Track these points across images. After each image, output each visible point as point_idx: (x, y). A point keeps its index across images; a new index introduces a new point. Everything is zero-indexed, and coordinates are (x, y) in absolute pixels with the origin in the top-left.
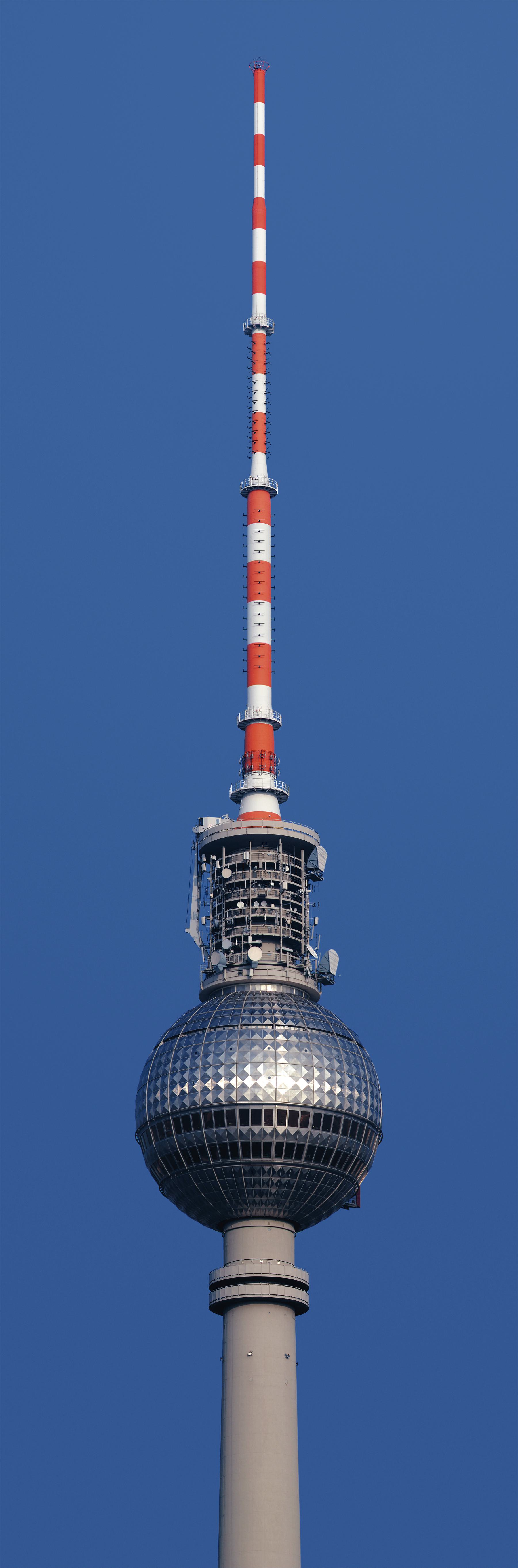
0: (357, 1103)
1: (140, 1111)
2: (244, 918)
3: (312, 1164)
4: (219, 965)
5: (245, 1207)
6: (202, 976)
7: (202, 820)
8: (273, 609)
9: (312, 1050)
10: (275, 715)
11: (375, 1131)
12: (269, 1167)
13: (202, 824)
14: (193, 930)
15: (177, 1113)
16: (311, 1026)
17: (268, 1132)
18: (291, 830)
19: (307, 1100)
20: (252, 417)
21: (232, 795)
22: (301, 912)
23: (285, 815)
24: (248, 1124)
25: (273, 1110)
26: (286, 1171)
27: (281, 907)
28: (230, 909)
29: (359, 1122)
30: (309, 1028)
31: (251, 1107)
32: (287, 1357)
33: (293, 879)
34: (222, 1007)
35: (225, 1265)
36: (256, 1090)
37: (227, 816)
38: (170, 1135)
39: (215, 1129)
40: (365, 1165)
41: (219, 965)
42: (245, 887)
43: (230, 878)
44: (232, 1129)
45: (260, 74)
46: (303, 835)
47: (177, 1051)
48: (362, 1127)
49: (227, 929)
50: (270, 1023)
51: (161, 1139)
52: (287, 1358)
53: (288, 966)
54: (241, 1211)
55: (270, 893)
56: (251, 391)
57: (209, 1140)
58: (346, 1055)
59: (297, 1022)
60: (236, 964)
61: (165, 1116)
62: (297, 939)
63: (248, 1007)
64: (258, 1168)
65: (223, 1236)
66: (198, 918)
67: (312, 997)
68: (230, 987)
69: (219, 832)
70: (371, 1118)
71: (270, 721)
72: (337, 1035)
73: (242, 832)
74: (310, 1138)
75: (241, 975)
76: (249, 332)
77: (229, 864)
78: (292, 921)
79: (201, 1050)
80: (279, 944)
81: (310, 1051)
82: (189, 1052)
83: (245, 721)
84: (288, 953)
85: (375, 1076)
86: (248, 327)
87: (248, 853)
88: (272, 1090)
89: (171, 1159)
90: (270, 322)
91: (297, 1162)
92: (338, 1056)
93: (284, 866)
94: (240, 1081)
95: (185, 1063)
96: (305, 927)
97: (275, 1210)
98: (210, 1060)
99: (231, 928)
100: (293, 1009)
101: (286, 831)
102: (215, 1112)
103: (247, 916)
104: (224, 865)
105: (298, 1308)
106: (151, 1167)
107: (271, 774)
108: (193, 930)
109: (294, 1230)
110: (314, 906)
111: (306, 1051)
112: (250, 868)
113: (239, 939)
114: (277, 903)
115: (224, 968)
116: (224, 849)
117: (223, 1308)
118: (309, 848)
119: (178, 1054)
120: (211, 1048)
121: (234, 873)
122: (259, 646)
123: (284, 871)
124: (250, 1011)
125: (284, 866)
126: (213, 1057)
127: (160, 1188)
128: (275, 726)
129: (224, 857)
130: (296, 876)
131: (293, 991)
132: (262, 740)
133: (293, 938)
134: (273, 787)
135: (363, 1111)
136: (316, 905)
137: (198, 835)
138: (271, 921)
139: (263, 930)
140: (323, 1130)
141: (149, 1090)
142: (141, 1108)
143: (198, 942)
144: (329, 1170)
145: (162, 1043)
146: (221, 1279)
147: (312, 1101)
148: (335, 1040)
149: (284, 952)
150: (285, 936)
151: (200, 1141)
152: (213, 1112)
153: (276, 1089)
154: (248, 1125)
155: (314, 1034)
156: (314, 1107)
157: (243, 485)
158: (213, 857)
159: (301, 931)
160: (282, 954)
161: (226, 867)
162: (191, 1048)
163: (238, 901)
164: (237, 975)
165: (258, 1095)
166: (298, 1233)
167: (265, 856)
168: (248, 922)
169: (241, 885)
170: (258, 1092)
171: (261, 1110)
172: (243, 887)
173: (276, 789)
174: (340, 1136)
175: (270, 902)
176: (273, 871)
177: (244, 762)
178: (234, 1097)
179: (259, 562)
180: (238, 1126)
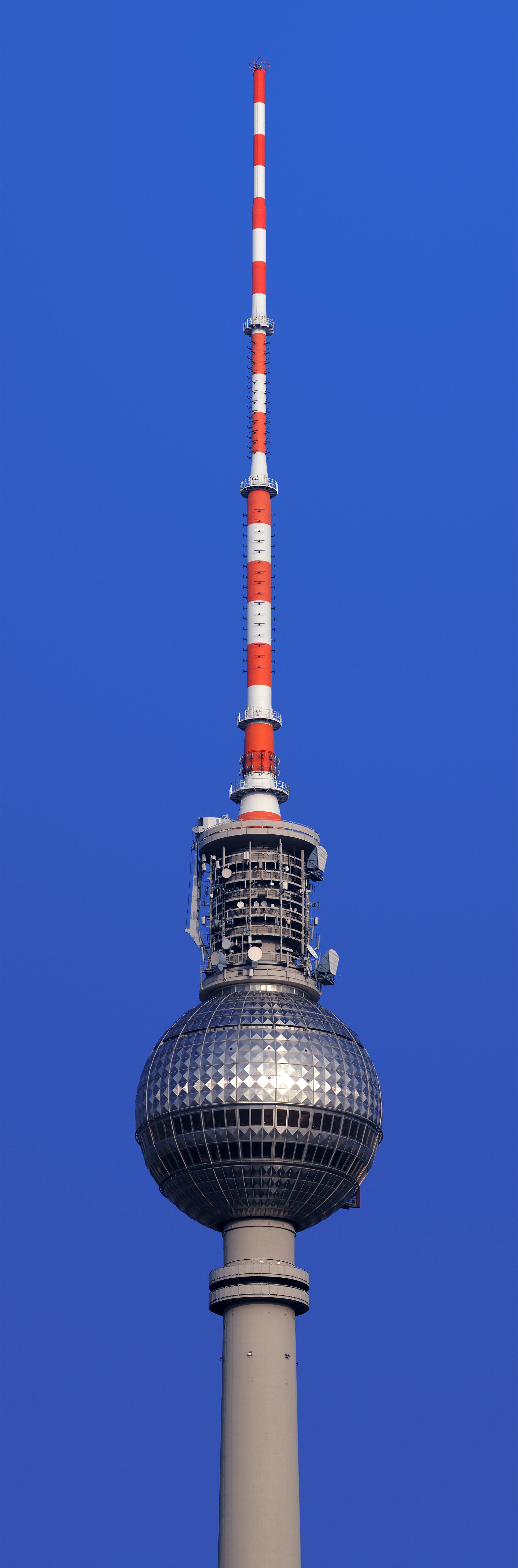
0: (357, 1102)
1: (140, 1111)
2: (244, 919)
3: (312, 1164)
4: (219, 965)
5: (245, 1207)
6: (202, 976)
7: (202, 820)
8: (273, 609)
9: (312, 1050)
10: (275, 715)
11: (375, 1131)
12: (269, 1167)
13: (202, 824)
14: (193, 930)
15: (177, 1113)
16: (311, 1026)
17: (268, 1132)
18: (291, 830)
19: (307, 1100)
20: (252, 417)
21: (232, 795)
22: (301, 912)
23: (285, 815)
24: (248, 1124)
25: (273, 1110)
26: (286, 1171)
27: (281, 907)
28: (230, 909)
29: (360, 1122)
30: (309, 1028)
31: (251, 1107)
32: (287, 1357)
33: (293, 879)
34: (222, 1007)
35: (225, 1265)
36: (256, 1090)
37: (227, 816)
38: (170, 1135)
39: (215, 1129)
40: (365, 1165)
41: (219, 965)
42: (245, 887)
43: (230, 878)
44: (232, 1129)
45: (260, 74)
46: (303, 835)
47: (177, 1051)
48: (362, 1127)
49: (227, 929)
50: (270, 1023)
51: (161, 1139)
52: (287, 1358)
53: (288, 965)
54: (241, 1210)
55: (270, 893)
56: (250, 391)
57: (209, 1139)
58: (346, 1055)
59: (297, 1022)
60: (236, 964)
61: (165, 1116)
62: (297, 939)
63: (248, 1007)
64: (258, 1168)
65: (223, 1236)
66: (198, 918)
67: (312, 996)
68: (230, 987)
69: (219, 832)
70: (371, 1118)
71: (270, 721)
72: (337, 1035)
73: (242, 832)
74: (310, 1138)
75: (241, 975)
77: (229, 864)
78: (292, 921)
79: (201, 1050)
80: (279, 944)
81: (310, 1051)
82: (189, 1052)
83: (245, 721)
84: (288, 953)
85: (375, 1076)
86: (248, 327)
87: (248, 853)
88: (272, 1090)
89: (171, 1160)
90: (270, 322)
91: (297, 1162)
92: (338, 1056)
93: (284, 866)
94: (240, 1081)
95: (184, 1076)
96: (305, 927)
97: (275, 1210)
98: (210, 1059)
99: (231, 928)
100: (294, 1009)
101: (286, 831)
102: (215, 1112)
103: (247, 916)
104: (224, 865)
105: (298, 1308)
106: (152, 1167)
107: (271, 774)
108: (193, 930)
109: (294, 1230)
110: (314, 906)
111: (306, 1051)
112: (250, 868)
113: (239, 939)
114: (277, 903)
115: (224, 968)
116: (224, 849)
117: (222, 1308)
118: (309, 849)
119: (178, 1054)
120: (211, 1048)
121: (234, 873)
122: (259, 646)
123: (284, 870)
124: (250, 1011)
125: (284, 866)
126: (213, 1057)
127: (160, 1188)
128: (276, 726)
129: (224, 857)
130: (296, 876)
131: (293, 991)
132: (262, 740)
133: (293, 938)
134: (273, 787)
135: (363, 1111)
136: (316, 905)
137: (198, 834)
138: (271, 921)
139: (263, 930)
140: (323, 1130)
141: (149, 1090)
142: (141, 1109)
143: (198, 942)
144: (328, 1170)
145: (162, 1043)
147: (312, 1101)
148: (335, 1040)
149: (284, 951)
150: (285, 936)
151: (200, 1141)
152: (190, 1116)
153: (276, 1089)
154: (248, 1124)
155: (314, 1034)
156: (314, 1107)
157: (243, 485)
158: (213, 857)
159: (301, 931)
160: (282, 954)
161: (226, 867)
162: (191, 1048)
163: (239, 901)
164: (237, 975)
165: (258, 1095)
166: (298, 1233)
167: (265, 856)
168: (248, 921)
169: (240, 885)
170: (258, 1092)
171: (261, 1110)
172: (243, 887)
173: (276, 789)
174: (340, 1136)
175: (270, 902)
176: (273, 871)
177: (244, 762)
178: (234, 1097)
179: (259, 562)
180: (238, 1126)
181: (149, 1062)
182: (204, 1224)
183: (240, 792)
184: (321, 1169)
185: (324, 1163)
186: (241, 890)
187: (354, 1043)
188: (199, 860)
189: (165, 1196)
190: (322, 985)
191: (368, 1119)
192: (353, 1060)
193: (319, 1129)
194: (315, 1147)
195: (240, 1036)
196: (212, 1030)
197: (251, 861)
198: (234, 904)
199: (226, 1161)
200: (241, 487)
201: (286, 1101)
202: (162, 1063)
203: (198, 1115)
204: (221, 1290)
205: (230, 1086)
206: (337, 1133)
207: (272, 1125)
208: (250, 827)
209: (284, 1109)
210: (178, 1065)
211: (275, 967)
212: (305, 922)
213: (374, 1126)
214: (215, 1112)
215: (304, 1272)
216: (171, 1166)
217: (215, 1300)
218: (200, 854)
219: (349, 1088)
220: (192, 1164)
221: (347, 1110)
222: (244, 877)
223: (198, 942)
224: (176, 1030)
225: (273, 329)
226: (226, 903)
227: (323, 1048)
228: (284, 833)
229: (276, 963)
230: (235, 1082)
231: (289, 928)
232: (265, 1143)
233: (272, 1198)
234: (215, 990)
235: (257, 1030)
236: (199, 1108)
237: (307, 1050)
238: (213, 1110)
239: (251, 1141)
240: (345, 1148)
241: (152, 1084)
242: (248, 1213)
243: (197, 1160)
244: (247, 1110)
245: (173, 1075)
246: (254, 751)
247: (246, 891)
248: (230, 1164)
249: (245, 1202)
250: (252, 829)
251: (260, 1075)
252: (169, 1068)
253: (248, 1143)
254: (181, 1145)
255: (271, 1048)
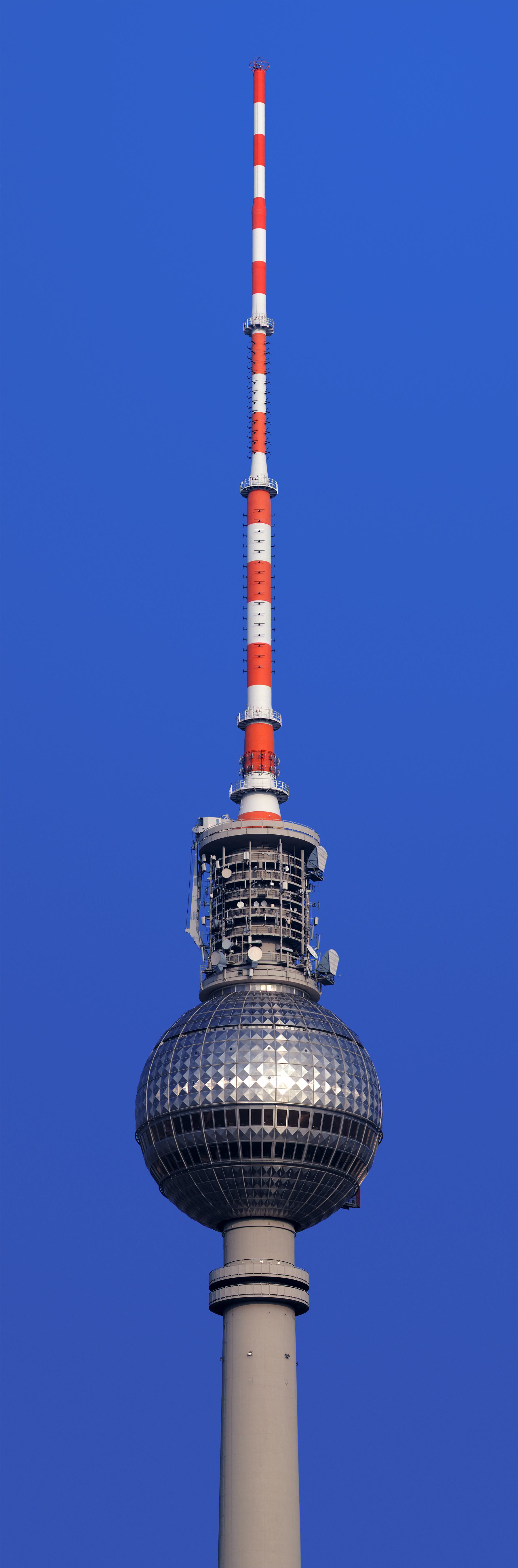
0: (357, 1102)
1: (140, 1111)
2: (244, 919)
3: (312, 1164)
4: (219, 965)
5: (245, 1207)
6: (202, 976)
7: (202, 820)
8: (273, 609)
9: (312, 1050)
10: (275, 715)
11: (375, 1131)
12: (269, 1167)
13: (202, 824)
14: (193, 930)
15: (177, 1113)
16: (311, 1026)
17: (268, 1132)
18: (291, 830)
19: (307, 1100)
20: (252, 417)
21: (232, 795)
22: (301, 912)
23: (285, 815)
24: (248, 1124)
25: (273, 1110)
26: (286, 1171)
27: (281, 907)
28: (230, 909)
29: (360, 1122)
30: (309, 1028)
31: (251, 1107)
32: (287, 1357)
33: (293, 879)
34: (222, 1007)
36: (256, 1090)
37: (227, 816)
38: (170, 1135)
39: (215, 1129)
40: (365, 1165)
41: (219, 965)
42: (245, 887)
43: (230, 878)
44: (232, 1129)
45: (260, 74)
46: (303, 835)
47: (177, 1051)
48: (362, 1127)
49: (227, 929)
50: (270, 1023)
51: (161, 1139)
53: (288, 965)
54: (241, 1210)
55: (270, 893)
56: (250, 391)
57: (209, 1139)
58: (346, 1055)
59: (297, 1022)
60: (236, 964)
61: (165, 1116)
62: (297, 939)
64: (258, 1168)
65: (223, 1236)
66: (198, 918)
67: (312, 996)
68: (230, 987)
69: (219, 832)
70: (371, 1118)
71: (270, 721)
73: (242, 832)
74: (310, 1138)
75: (241, 975)
76: (249, 332)
77: (229, 864)
78: (292, 921)
79: (201, 1050)
80: (279, 944)
81: (310, 1051)
82: (189, 1052)
83: (245, 721)
84: (288, 953)
85: (375, 1076)
86: (248, 327)
87: (248, 853)
88: (272, 1090)
89: (171, 1160)
90: (270, 322)
91: (297, 1162)
92: (338, 1056)
93: (284, 866)
94: (240, 1081)
95: (184, 1076)
96: (305, 927)
97: (275, 1210)
98: (210, 1059)
99: (231, 928)
100: (294, 1009)
102: (215, 1112)
103: (247, 916)
104: (224, 865)
105: (298, 1308)
106: (152, 1167)
107: (271, 774)
108: (193, 930)
109: (294, 1230)
110: (314, 906)
111: (306, 1051)
112: (250, 868)
113: (239, 939)
114: (277, 903)
115: (224, 968)
116: (224, 849)
117: (222, 1308)
118: (309, 849)
119: (178, 1054)
120: (211, 1048)
121: (234, 873)
122: (259, 646)
123: (284, 870)
124: (250, 1011)
125: (284, 866)
126: (213, 1057)
127: (160, 1188)
128: (276, 726)
129: (224, 857)
130: (296, 876)
131: (293, 991)
132: (262, 740)
133: (293, 938)
134: (273, 787)
135: (363, 1111)
136: (316, 905)
137: (198, 834)
138: (271, 921)
139: (263, 930)
140: (323, 1130)
141: (149, 1090)
142: (141, 1109)
143: (198, 942)
144: (328, 1170)
145: (162, 1043)
146: (221, 1300)
147: (312, 1101)
148: (335, 1040)
149: (284, 951)
150: (285, 936)
151: (200, 1141)
152: (190, 1116)
153: (276, 1089)
154: (248, 1124)
155: (314, 1034)
156: (314, 1107)
157: (243, 485)
158: (213, 857)
159: (301, 931)
160: (282, 954)
161: (226, 867)
162: (191, 1048)
163: (239, 901)
164: (237, 975)
165: (258, 1095)
166: (298, 1233)
167: (265, 856)
168: (248, 921)
169: (240, 885)
170: (258, 1092)
171: (261, 1110)
172: (243, 887)
173: (276, 789)
174: (340, 1136)
175: (270, 902)
176: (273, 871)
177: (244, 762)
178: (234, 1097)
179: (259, 562)
180: (238, 1126)
181: (149, 1062)
182: (204, 1224)
183: (240, 792)
184: (321, 1169)
185: (324, 1163)
186: (241, 890)
187: (354, 1043)
188: (199, 860)
189: (165, 1196)
190: (322, 985)
191: (368, 1119)
192: (353, 1060)
193: (319, 1129)
194: (315, 1147)
195: (240, 1036)
196: (212, 1030)
197: (251, 861)
198: (234, 904)
199: (226, 1161)
200: (241, 487)
201: (286, 1101)
202: (162, 1063)
203: (198, 1115)
204: (221, 1290)
205: (230, 1086)
206: (337, 1133)
207: (272, 1125)
208: (250, 827)
209: (284, 1109)
210: (178, 1065)
211: (275, 967)
212: (305, 922)
213: (374, 1126)
214: (215, 1112)
215: (304, 1272)
216: (171, 1166)
217: (215, 1300)
218: (200, 854)
219: (349, 1088)
220: (192, 1164)
221: (347, 1110)
222: (244, 877)
223: (198, 942)
224: (176, 1030)
225: (273, 329)
226: (226, 903)
227: (323, 1048)
228: (284, 833)
229: (276, 963)
230: (235, 1082)
231: (289, 928)
232: (265, 1143)
233: (272, 1198)
234: (215, 990)
235: (257, 1030)
236: (199, 1108)
237: (307, 1050)
238: (213, 1110)
239: (251, 1141)
240: (345, 1148)
241: (152, 1084)
242: (248, 1213)
243: (197, 1160)
244: (247, 1110)
245: (173, 1075)
246: (254, 751)
247: (246, 891)
248: (230, 1164)
249: (245, 1202)
250: (252, 829)
251: (260, 1075)
252: (169, 1068)
253: (248, 1143)
254: (181, 1145)
255: (271, 1048)
